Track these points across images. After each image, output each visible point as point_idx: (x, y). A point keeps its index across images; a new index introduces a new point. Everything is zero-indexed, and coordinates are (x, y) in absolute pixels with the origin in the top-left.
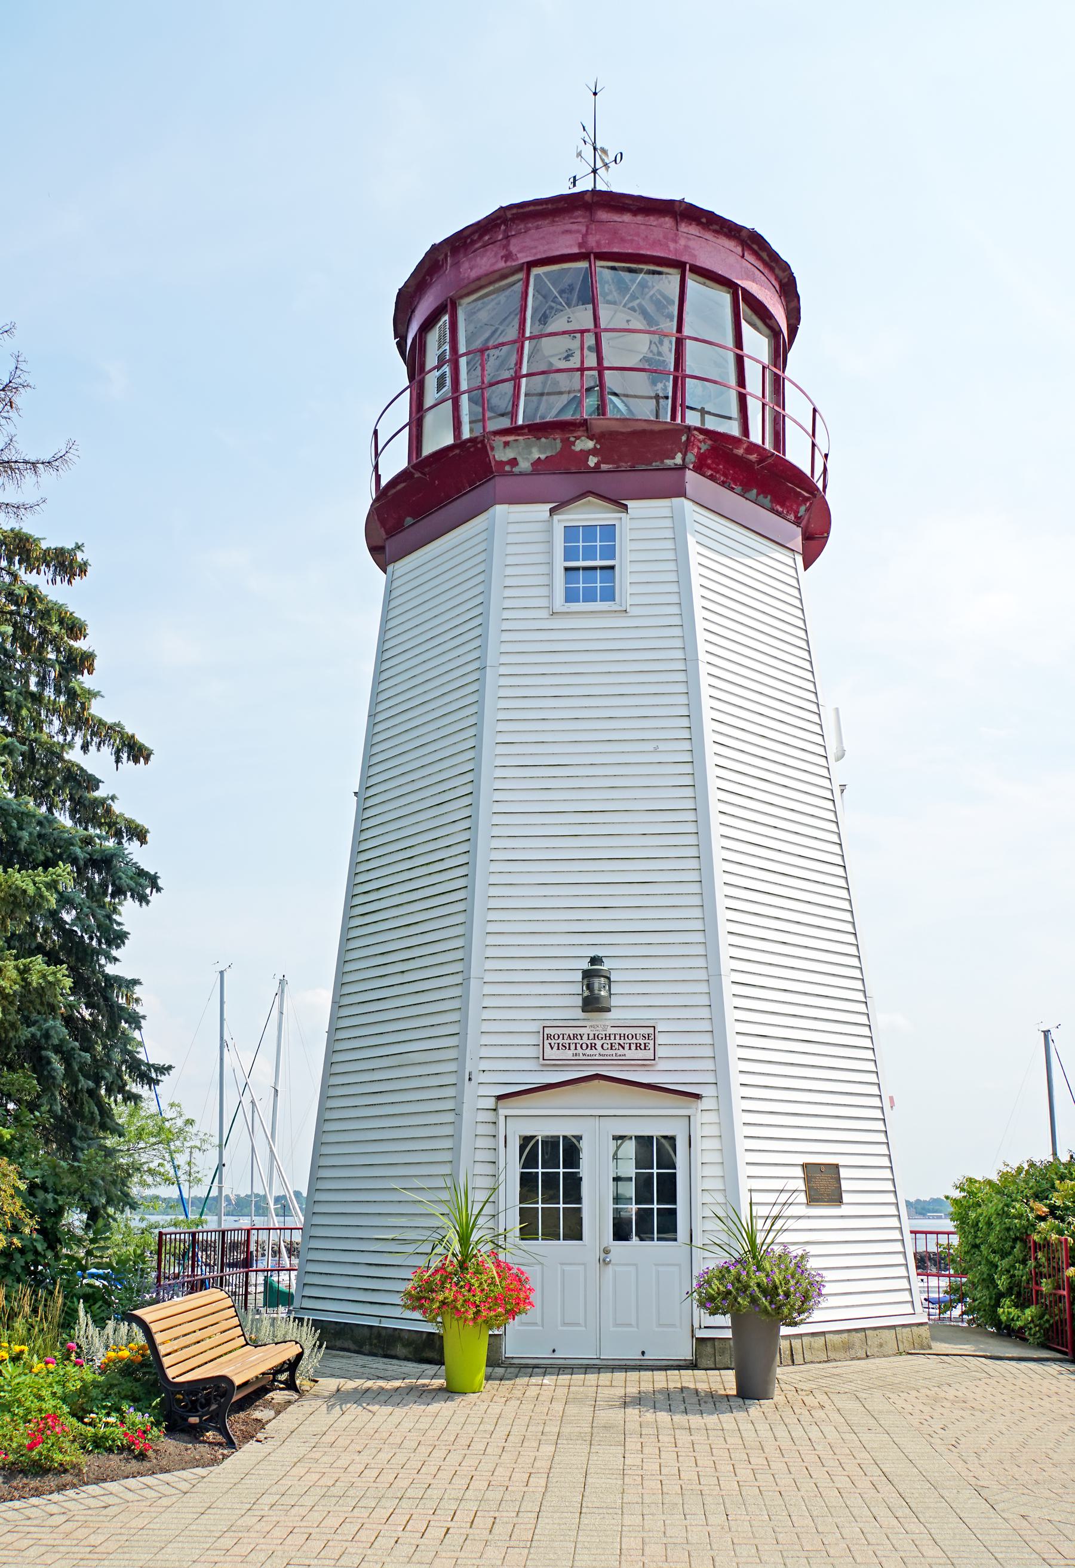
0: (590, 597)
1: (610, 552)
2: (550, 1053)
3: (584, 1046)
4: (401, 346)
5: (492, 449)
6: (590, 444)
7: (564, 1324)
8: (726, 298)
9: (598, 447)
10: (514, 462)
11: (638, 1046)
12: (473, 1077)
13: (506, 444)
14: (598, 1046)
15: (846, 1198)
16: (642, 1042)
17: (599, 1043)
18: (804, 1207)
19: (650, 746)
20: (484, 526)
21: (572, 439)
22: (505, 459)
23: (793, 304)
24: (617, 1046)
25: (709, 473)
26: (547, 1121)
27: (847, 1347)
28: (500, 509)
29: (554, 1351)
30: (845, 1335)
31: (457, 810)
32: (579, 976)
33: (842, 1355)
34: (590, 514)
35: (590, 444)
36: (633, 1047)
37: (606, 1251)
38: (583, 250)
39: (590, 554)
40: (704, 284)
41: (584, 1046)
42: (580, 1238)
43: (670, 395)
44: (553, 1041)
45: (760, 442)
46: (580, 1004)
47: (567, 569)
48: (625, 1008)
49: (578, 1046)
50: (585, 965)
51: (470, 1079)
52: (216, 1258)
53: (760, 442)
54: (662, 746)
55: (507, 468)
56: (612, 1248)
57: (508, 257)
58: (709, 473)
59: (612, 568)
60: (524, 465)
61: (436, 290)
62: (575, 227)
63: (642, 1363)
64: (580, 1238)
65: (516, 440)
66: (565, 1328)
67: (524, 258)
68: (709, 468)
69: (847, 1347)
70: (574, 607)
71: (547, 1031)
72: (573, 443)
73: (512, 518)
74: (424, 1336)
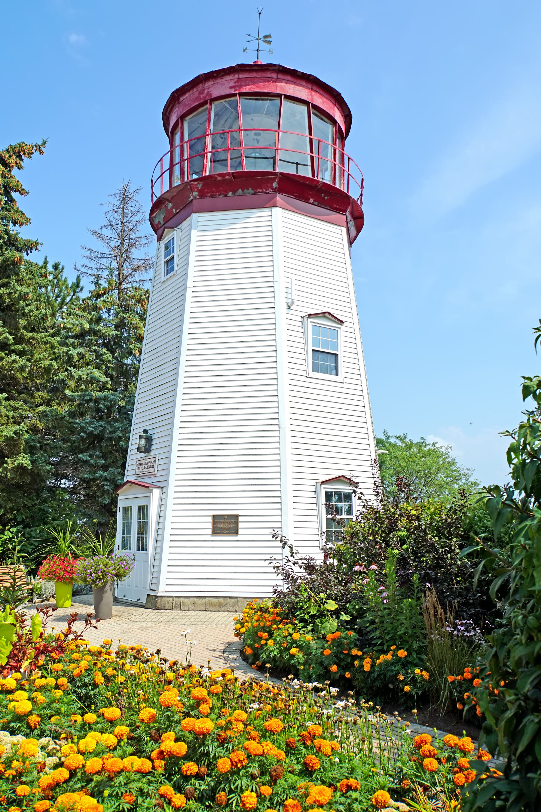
4: (167, 134)
8: (305, 108)
15: (240, 531)
20: (189, 223)
23: (347, 113)
25: (209, 195)
27: (221, 605)
28: (194, 215)
30: (222, 599)
31: (169, 366)
33: (217, 609)
40: (256, 99)
45: (310, 176)
52: (528, 420)
53: (310, 176)
58: (209, 195)
61: (185, 104)
68: (208, 193)
69: (221, 605)
73: (200, 219)
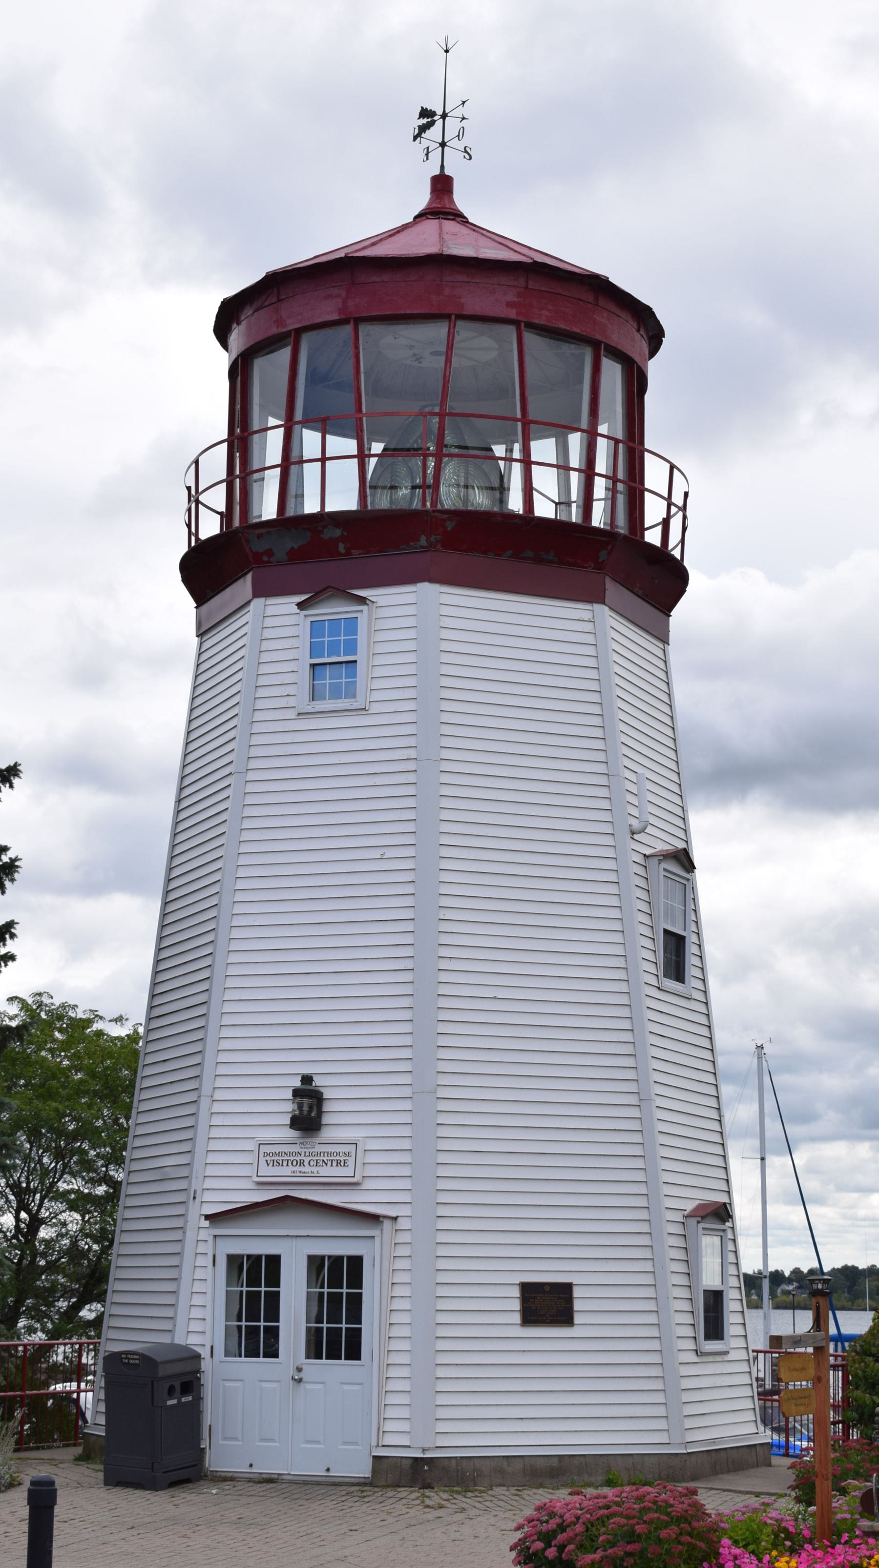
0: (336, 693)
1: (352, 647)
2: (265, 1170)
3: (295, 1163)
5: (248, 541)
6: (338, 532)
7: (262, 1440)
9: (346, 534)
10: (270, 553)
11: (338, 1163)
12: (197, 1197)
13: (260, 536)
14: (306, 1163)
15: (577, 1319)
16: (342, 1159)
17: (307, 1160)
18: (518, 1327)
19: (376, 854)
21: (320, 528)
22: (261, 550)
24: (321, 1163)
26: (253, 1240)
29: (251, 1465)
32: (289, 1095)
34: (332, 610)
35: (338, 532)
36: (335, 1163)
37: (299, 1370)
38: (343, 317)
39: (334, 648)
41: (295, 1163)
42: (276, 1356)
43: (368, 490)
44: (268, 1158)
46: (288, 1122)
47: (313, 666)
48: (339, 1124)
49: (290, 1163)
50: (297, 1083)
51: (194, 1198)
54: (390, 853)
55: (265, 558)
56: (304, 1367)
57: (279, 322)
59: (355, 661)
60: (280, 554)
62: (335, 291)
63: (328, 1479)
64: (276, 1356)
65: (268, 533)
66: (345, 1447)
67: (292, 325)
70: (320, 706)
71: (264, 1149)
72: (322, 532)
74: (409, 1462)
